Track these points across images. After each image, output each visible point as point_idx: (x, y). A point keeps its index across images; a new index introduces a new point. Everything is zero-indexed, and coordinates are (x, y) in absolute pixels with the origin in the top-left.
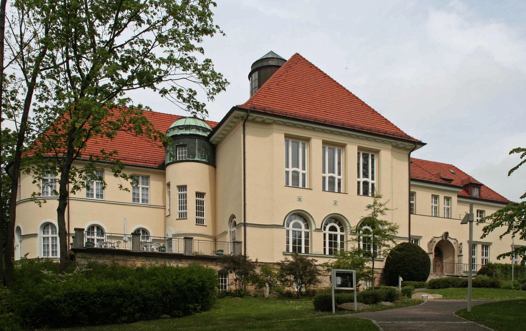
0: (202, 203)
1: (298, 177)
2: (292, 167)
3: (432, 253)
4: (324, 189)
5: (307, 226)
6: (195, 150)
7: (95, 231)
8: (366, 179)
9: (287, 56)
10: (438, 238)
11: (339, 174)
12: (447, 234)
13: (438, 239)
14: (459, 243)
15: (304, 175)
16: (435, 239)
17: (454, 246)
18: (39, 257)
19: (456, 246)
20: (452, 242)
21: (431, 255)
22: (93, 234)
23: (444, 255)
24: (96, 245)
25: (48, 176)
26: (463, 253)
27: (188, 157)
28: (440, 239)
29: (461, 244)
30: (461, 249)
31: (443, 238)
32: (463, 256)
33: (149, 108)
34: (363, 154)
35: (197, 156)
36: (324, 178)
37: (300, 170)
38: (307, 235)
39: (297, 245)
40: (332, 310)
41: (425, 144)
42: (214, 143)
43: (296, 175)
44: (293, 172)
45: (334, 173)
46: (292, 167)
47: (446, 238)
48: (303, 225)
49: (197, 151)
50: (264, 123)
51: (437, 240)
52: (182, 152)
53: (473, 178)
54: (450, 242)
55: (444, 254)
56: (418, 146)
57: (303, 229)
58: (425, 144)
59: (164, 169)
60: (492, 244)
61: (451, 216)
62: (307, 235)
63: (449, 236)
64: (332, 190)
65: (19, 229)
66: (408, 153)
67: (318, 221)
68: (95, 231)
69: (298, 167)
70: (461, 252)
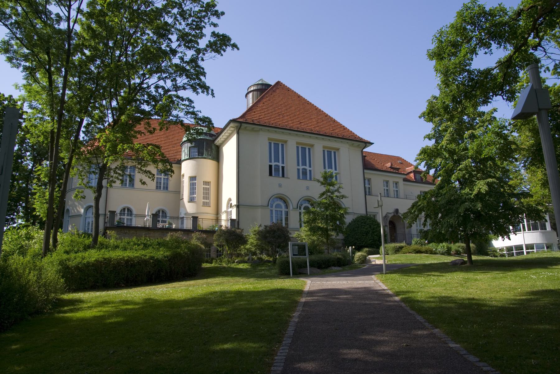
0: (208, 189)
1: (279, 169)
2: (274, 162)
3: (387, 226)
4: (299, 178)
5: (287, 207)
6: (203, 150)
7: (126, 212)
8: (304, 167)
9: (273, 83)
11: (310, 166)
15: (310, 171)
22: (124, 214)
24: (126, 223)
25: (161, 175)
27: (198, 155)
28: (392, 215)
34: (282, 144)
35: (204, 155)
36: (298, 170)
37: (307, 168)
38: (287, 213)
40: (290, 274)
41: (372, 144)
42: (217, 144)
43: (305, 172)
44: (275, 165)
45: (306, 165)
46: (274, 162)
48: (283, 205)
49: (205, 150)
50: (253, 130)
51: (390, 216)
52: (194, 152)
56: (367, 145)
57: (284, 209)
58: (372, 144)
59: (181, 164)
62: (287, 213)
64: (277, 175)
65: (68, 210)
66: (361, 149)
67: (293, 203)
68: (126, 212)
69: (279, 162)
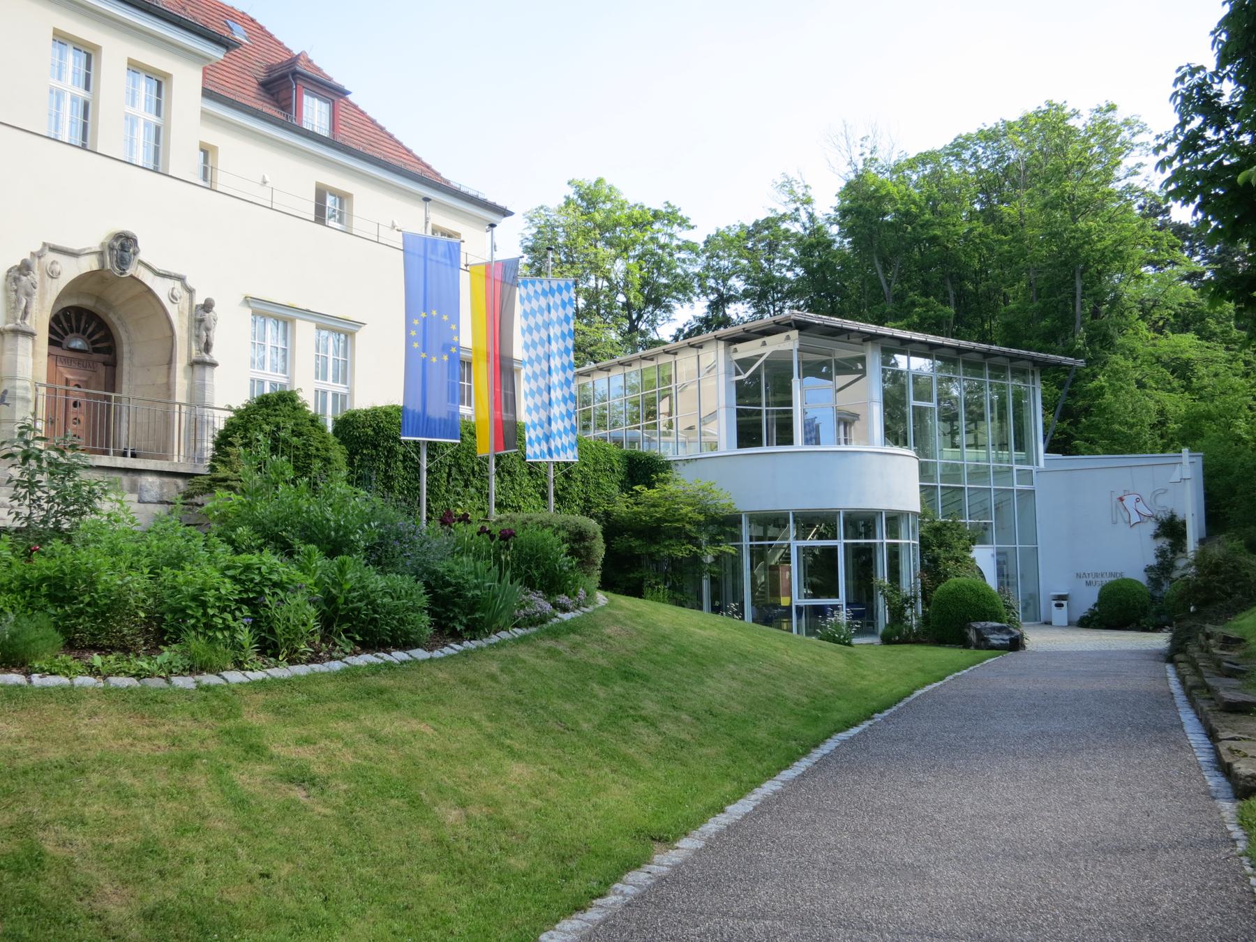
10: (74, 254)
12: (123, 245)
13: (73, 260)
14: (199, 300)
16: (51, 257)
17: (172, 310)
18: (338, 440)
19: (181, 313)
20: (161, 288)
21: (24, 344)
23: (126, 355)
26: (215, 354)
28: (89, 264)
29: (208, 306)
30: (208, 329)
31: (102, 263)
32: (217, 368)
33: (473, 434)
39: (1018, 546)
47: (123, 263)
51: (71, 270)
53: (310, 61)
54: (149, 290)
55: (126, 348)
60: (364, 328)
61: (167, 164)
63: (142, 256)
70: (207, 347)
